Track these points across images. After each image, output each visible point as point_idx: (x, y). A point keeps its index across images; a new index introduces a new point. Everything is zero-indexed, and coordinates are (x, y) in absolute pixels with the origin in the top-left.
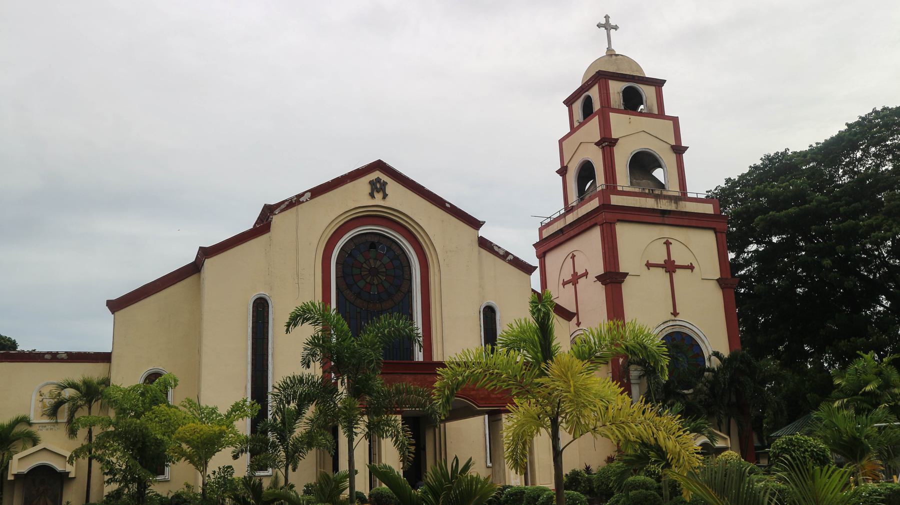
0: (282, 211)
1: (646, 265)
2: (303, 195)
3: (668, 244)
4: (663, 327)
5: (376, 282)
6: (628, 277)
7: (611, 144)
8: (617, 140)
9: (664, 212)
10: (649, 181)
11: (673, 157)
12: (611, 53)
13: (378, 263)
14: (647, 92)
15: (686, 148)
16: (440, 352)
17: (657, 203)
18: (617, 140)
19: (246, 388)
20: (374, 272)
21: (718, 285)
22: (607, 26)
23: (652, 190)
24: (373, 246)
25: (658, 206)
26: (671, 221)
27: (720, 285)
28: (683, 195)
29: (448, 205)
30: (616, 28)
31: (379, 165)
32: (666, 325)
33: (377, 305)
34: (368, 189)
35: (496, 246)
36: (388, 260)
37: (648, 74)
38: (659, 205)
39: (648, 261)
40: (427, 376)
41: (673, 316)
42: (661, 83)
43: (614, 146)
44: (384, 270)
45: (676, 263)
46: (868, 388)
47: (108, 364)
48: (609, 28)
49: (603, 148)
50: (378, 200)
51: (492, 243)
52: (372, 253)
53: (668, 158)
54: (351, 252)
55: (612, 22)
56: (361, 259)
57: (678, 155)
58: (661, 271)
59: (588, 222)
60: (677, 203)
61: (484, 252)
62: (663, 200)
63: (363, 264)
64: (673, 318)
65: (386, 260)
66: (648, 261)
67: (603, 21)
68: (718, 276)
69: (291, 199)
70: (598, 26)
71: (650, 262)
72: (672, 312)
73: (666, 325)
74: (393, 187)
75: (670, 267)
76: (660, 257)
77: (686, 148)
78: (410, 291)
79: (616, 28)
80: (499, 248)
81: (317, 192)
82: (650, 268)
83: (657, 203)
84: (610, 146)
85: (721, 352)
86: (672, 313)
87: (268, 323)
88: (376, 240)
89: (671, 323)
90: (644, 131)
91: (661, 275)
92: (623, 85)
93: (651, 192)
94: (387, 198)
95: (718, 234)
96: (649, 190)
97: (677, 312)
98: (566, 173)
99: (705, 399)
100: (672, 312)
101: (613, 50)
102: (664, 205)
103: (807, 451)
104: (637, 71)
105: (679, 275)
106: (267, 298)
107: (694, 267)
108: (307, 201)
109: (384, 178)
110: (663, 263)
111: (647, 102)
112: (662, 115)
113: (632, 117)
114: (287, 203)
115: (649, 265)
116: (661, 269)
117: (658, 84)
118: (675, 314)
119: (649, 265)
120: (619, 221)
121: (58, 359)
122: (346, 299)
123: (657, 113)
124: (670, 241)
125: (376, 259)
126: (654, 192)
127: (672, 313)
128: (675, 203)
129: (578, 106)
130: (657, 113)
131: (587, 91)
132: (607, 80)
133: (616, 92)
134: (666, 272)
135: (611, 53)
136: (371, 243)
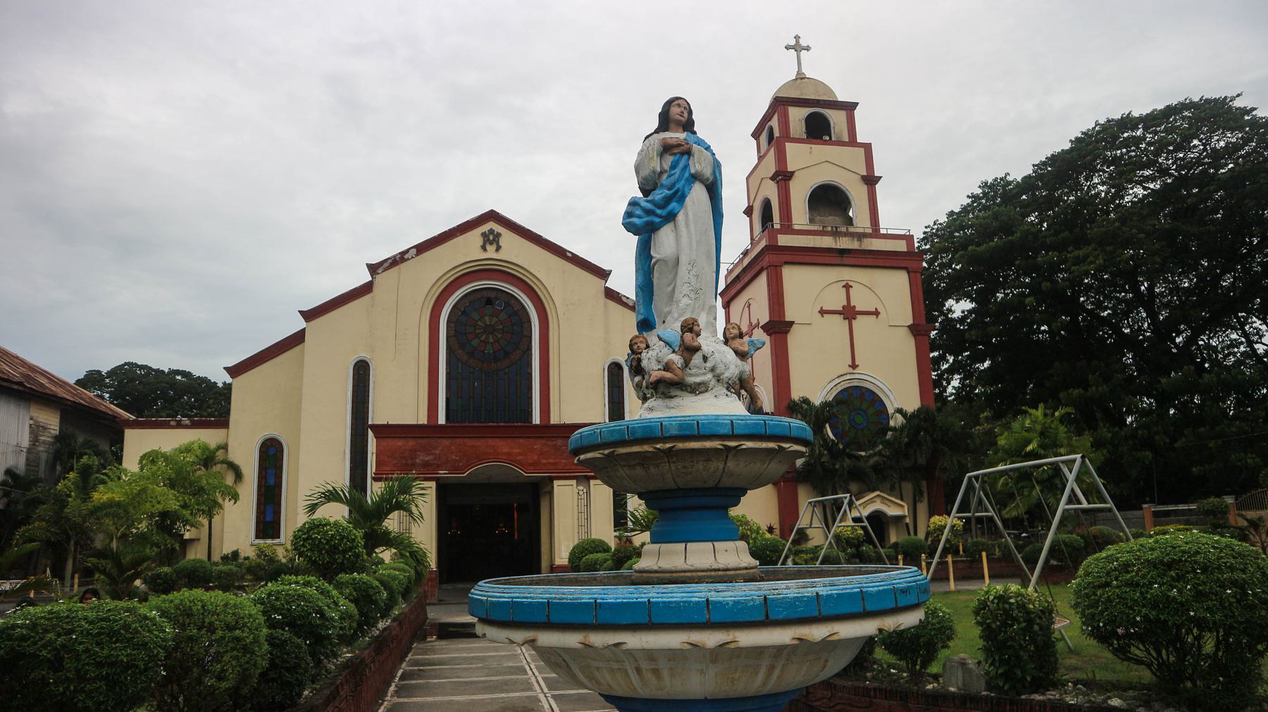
0: (386, 269)
1: (819, 312)
2: (407, 251)
3: (847, 287)
4: (838, 381)
5: (491, 340)
6: (794, 325)
7: (785, 178)
8: (792, 173)
9: (842, 252)
10: (837, 218)
11: (864, 189)
12: (801, 77)
13: (495, 320)
14: (837, 119)
15: (880, 178)
16: (557, 413)
17: (836, 242)
18: (792, 173)
19: (344, 453)
20: (490, 329)
21: (910, 332)
22: (797, 47)
23: (836, 228)
24: (489, 302)
25: (836, 245)
26: (851, 261)
27: (912, 332)
28: (876, 233)
29: (569, 254)
30: (808, 48)
31: (492, 216)
32: (842, 379)
33: (493, 365)
34: (480, 241)
35: (624, 296)
36: (506, 316)
37: (841, 97)
38: (838, 243)
39: (822, 308)
40: (466, 440)
41: (851, 369)
42: (855, 105)
43: (790, 180)
44: (501, 327)
45: (857, 309)
46: (1030, 448)
47: (226, 430)
48: (799, 50)
49: (777, 182)
50: (491, 252)
51: (619, 293)
52: (489, 309)
53: (857, 193)
54: (464, 310)
55: (803, 43)
56: (475, 315)
57: (870, 186)
58: (838, 319)
59: (871, 260)
60: (861, 241)
61: (612, 304)
62: (844, 238)
63: (497, 317)
64: (851, 370)
65: (503, 316)
66: (822, 308)
67: (793, 42)
68: (910, 322)
69: (394, 256)
70: (786, 48)
71: (824, 308)
72: (851, 364)
73: (842, 379)
74: (507, 237)
75: (849, 313)
76: (838, 302)
77: (880, 178)
78: (529, 348)
79: (808, 48)
80: (628, 298)
81: (422, 248)
82: (824, 315)
83: (836, 242)
84: (785, 180)
85: (904, 409)
86: (849, 366)
87: (369, 386)
88: (493, 295)
89: (848, 377)
90: (827, 161)
91: (839, 323)
92: (805, 112)
93: (834, 229)
94: (501, 251)
95: (910, 273)
96: (832, 227)
97: (857, 364)
98: (752, 214)
99: (884, 462)
100: (851, 364)
101: (804, 74)
102: (845, 243)
103: (198, 500)
104: (825, 95)
105: (859, 322)
106: (368, 361)
107: (879, 313)
108: (412, 257)
109: (498, 228)
110: (841, 309)
111: (836, 128)
112: (853, 142)
113: (813, 146)
114: (390, 261)
115: (823, 312)
116: (838, 315)
117: (850, 107)
118: (854, 366)
119: (823, 312)
120: (786, 263)
121: (183, 425)
122: (458, 360)
123: (847, 140)
124: (850, 283)
125: (492, 316)
126: (838, 230)
127: (849, 366)
128: (858, 240)
129: (764, 137)
130: (847, 140)
131: (769, 121)
132: (786, 106)
133: (797, 120)
134: (844, 319)
135: (801, 77)
136: (487, 299)
